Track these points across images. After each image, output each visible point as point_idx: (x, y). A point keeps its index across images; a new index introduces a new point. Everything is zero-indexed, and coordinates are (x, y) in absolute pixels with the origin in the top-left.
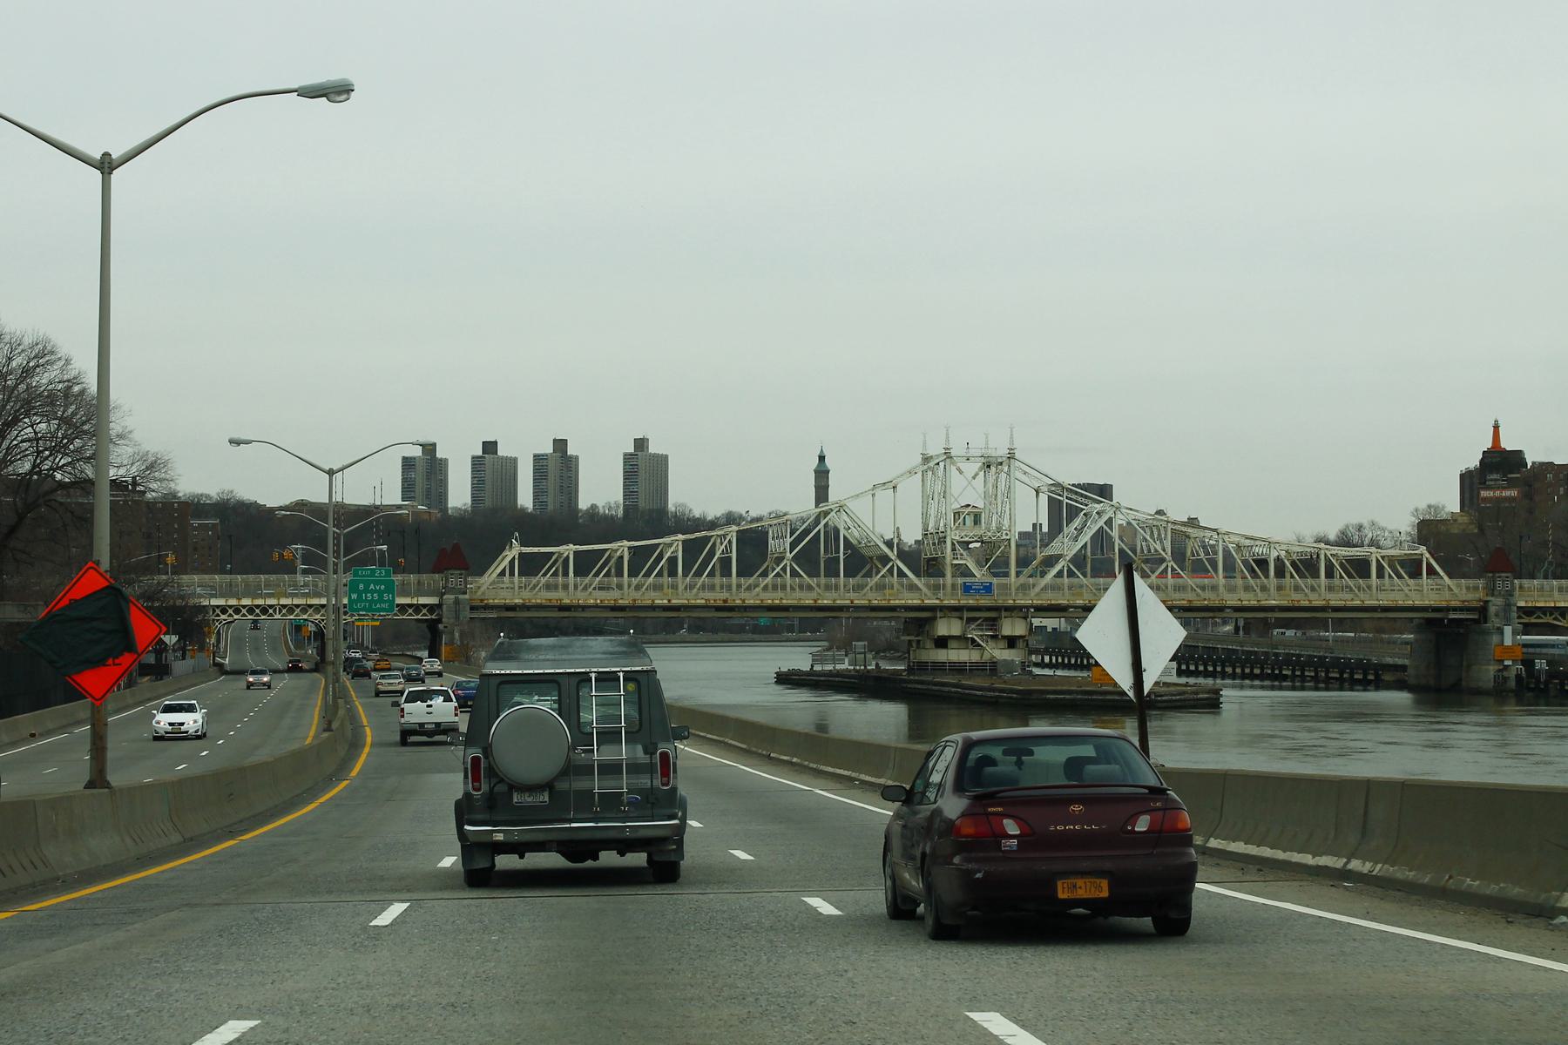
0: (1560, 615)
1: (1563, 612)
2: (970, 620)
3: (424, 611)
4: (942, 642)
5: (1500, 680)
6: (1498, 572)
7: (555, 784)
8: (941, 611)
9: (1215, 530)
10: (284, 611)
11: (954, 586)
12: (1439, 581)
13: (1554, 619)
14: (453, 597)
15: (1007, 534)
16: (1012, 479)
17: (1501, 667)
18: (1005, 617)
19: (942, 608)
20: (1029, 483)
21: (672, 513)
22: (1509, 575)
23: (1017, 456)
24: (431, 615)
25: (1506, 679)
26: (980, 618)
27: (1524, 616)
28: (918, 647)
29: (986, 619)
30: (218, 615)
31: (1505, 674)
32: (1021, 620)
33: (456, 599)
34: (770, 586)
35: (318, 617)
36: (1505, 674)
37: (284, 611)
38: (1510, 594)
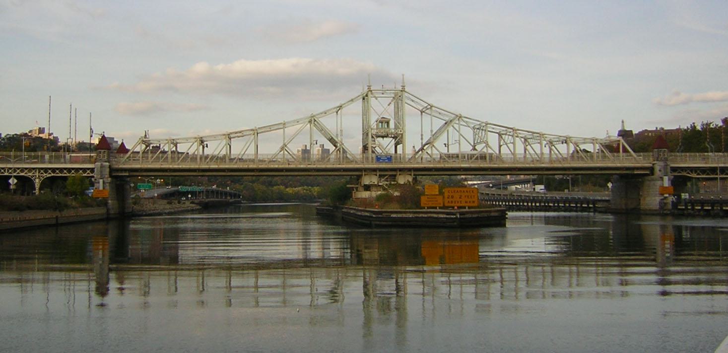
0: (690, 171)
1: (723, 170)
2: (380, 176)
3: (88, 172)
4: (367, 188)
5: (663, 204)
6: (661, 148)
7: (548, 161)
8: (365, 171)
9: (511, 129)
10: (10, 171)
11: (623, 159)
12: (629, 154)
13: (687, 173)
14: (100, 164)
15: (401, 131)
16: (404, 103)
17: (662, 198)
18: (400, 175)
19: (366, 170)
20: (415, 106)
21: (561, 158)
22: (666, 150)
23: (406, 90)
24: (85, 173)
25: (666, 204)
26: (387, 175)
27: (700, 173)
28: (357, 190)
29: (390, 176)
30: (42, 173)
31: (665, 201)
32: (409, 176)
33: (102, 164)
34: (479, 157)
35: (31, 174)
36: (665, 201)
37: (10, 171)
38: (666, 160)
